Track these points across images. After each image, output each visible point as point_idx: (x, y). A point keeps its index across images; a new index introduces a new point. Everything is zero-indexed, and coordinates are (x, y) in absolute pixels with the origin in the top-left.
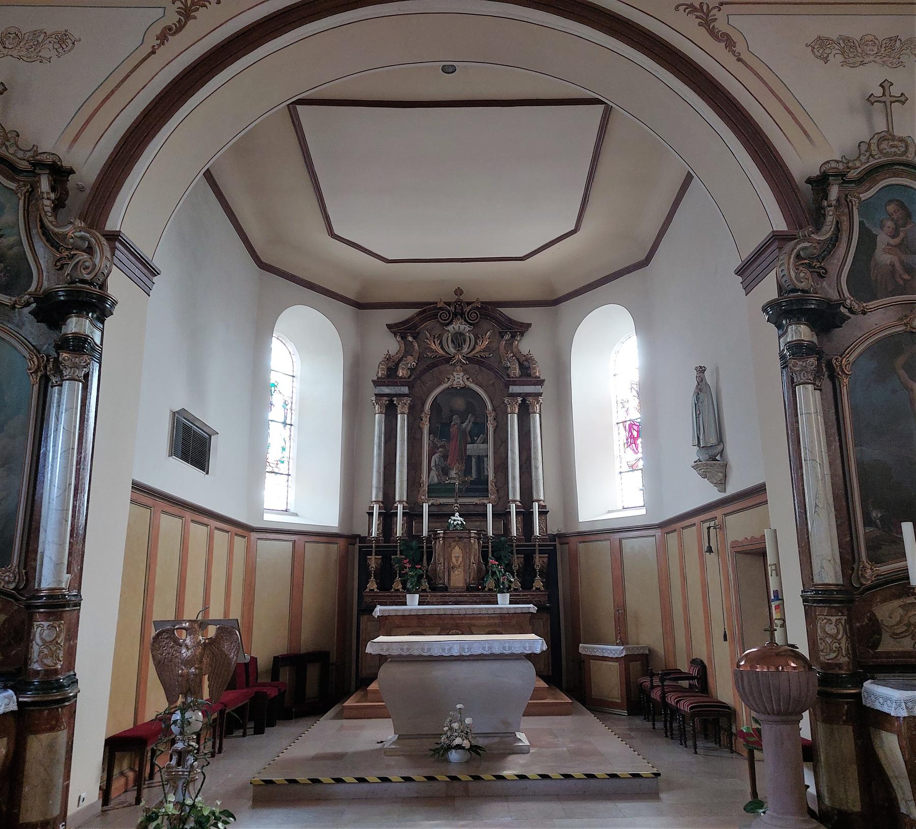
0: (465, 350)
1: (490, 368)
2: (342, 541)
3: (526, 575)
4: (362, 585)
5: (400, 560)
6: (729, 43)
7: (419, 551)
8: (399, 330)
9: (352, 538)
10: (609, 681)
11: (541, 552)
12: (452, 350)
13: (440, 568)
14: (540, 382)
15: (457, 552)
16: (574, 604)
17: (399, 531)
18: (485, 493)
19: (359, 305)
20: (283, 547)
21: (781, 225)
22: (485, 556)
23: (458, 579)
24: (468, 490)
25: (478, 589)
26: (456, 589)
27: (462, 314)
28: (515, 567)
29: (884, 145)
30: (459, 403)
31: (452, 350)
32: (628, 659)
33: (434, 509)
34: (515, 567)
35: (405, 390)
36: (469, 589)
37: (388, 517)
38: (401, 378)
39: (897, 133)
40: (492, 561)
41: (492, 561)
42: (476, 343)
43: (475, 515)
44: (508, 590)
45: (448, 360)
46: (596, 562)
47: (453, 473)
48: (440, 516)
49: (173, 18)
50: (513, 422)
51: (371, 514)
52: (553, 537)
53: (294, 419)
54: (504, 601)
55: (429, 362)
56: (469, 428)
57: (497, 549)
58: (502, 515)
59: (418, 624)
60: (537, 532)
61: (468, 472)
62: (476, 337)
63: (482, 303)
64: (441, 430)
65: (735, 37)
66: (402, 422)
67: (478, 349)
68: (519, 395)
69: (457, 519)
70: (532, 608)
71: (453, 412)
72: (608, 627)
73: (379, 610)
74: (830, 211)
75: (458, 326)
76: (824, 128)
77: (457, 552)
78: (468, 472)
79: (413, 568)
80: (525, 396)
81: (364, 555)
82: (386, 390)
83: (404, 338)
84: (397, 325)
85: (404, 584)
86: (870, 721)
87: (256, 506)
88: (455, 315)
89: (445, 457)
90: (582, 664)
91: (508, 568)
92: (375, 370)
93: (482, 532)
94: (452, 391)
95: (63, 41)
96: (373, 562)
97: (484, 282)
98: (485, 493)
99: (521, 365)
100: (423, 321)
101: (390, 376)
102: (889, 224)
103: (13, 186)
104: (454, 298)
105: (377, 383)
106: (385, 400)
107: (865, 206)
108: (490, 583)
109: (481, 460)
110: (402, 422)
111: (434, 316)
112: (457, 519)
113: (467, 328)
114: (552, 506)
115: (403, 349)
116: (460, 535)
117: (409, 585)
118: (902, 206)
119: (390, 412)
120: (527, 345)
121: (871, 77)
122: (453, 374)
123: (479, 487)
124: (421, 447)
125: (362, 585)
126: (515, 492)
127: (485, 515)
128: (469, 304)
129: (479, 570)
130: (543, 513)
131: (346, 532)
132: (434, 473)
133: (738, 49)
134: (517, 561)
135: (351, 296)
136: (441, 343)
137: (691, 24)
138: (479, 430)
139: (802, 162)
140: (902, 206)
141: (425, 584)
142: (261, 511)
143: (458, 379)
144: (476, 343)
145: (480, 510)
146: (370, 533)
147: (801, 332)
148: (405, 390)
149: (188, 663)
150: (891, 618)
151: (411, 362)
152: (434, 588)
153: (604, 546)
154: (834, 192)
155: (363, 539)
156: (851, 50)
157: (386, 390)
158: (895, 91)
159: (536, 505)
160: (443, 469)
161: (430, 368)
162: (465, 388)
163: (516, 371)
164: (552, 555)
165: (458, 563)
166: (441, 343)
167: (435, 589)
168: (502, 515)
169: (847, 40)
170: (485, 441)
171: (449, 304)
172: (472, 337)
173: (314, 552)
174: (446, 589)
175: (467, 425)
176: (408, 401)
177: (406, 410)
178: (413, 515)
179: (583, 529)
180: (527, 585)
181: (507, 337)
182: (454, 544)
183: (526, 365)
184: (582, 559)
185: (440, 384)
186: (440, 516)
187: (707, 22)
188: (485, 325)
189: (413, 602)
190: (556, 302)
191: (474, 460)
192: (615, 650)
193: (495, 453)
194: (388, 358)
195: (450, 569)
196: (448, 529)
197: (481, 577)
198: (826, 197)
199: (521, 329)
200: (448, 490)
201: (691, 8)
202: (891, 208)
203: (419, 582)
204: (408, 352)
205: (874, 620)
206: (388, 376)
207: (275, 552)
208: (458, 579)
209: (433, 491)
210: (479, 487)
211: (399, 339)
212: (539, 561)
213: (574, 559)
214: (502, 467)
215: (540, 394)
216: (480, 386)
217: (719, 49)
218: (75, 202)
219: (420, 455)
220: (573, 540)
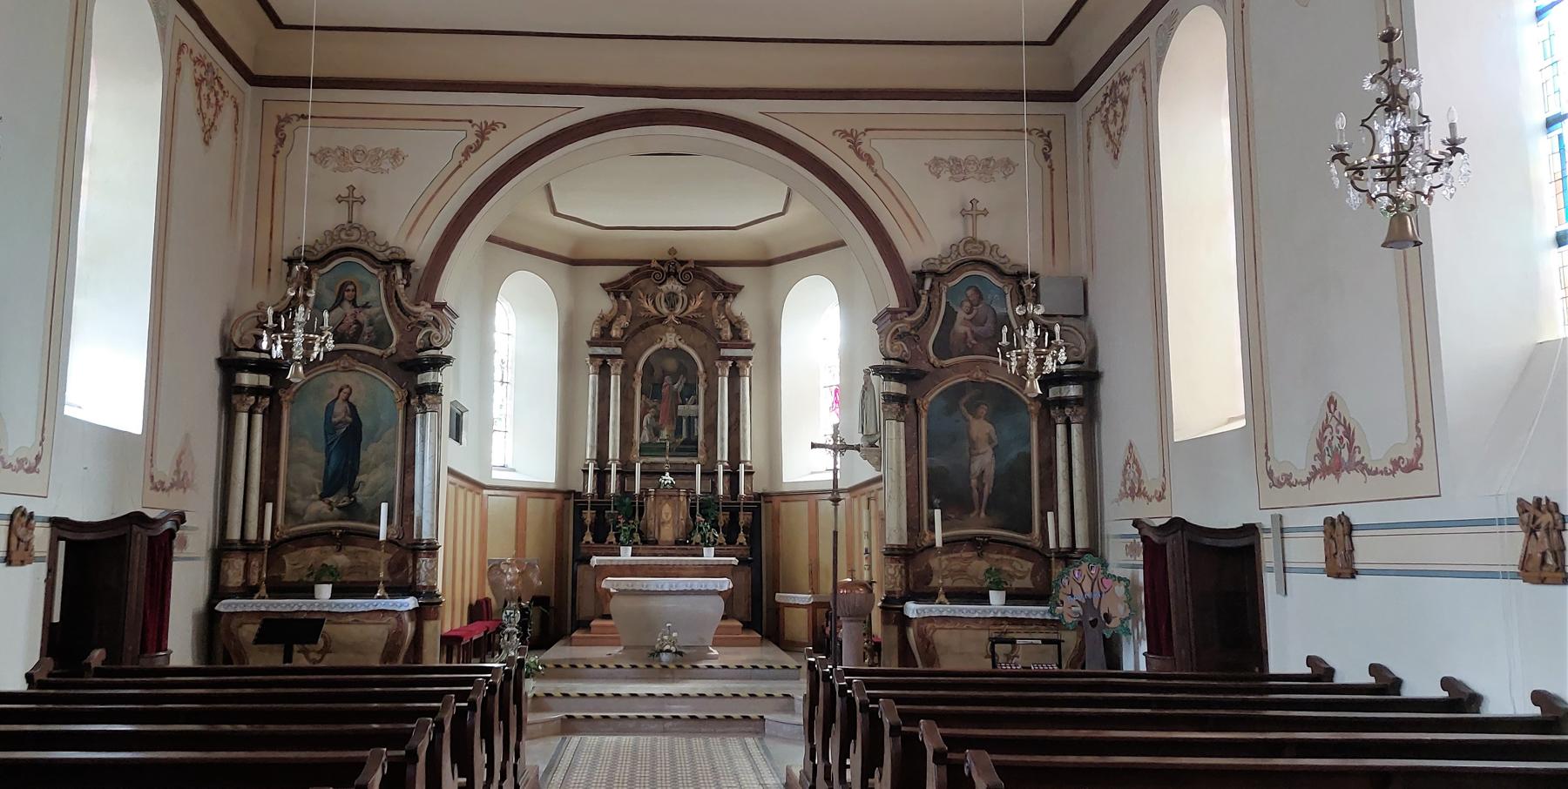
0: (678, 310)
1: (703, 330)
2: (559, 497)
3: (731, 532)
4: (578, 538)
5: (612, 515)
6: (870, 161)
7: (632, 507)
8: (616, 289)
9: (568, 494)
10: (798, 625)
11: (745, 510)
12: (665, 311)
13: (651, 523)
14: (751, 346)
15: (667, 509)
16: (775, 558)
17: (613, 487)
18: (694, 452)
19: (574, 262)
20: (510, 502)
21: (895, 304)
22: (693, 512)
23: (667, 534)
24: (679, 450)
25: (685, 543)
27: (676, 274)
28: (721, 524)
29: (969, 246)
30: (671, 364)
31: (665, 311)
32: (815, 606)
33: (646, 468)
34: (721, 524)
35: (618, 351)
36: (677, 543)
37: (602, 475)
39: (980, 237)
40: (699, 518)
41: (699, 518)
43: (685, 473)
44: (714, 544)
45: (661, 320)
46: (795, 518)
47: (664, 434)
48: (651, 473)
49: (472, 140)
50: (724, 384)
51: (586, 472)
52: (759, 496)
53: (509, 377)
54: (709, 554)
55: (641, 322)
57: (703, 507)
58: (710, 474)
59: (633, 570)
60: (742, 492)
61: (678, 432)
64: (653, 391)
65: (874, 156)
66: (615, 382)
68: (730, 358)
70: (734, 561)
72: (805, 581)
73: (595, 560)
74: (924, 298)
75: (672, 285)
76: (929, 236)
77: (667, 509)
78: (678, 432)
79: (627, 523)
80: (735, 360)
81: (579, 509)
82: (600, 351)
83: (617, 296)
84: (610, 284)
85: (617, 536)
86: (905, 621)
87: (486, 464)
88: (669, 274)
89: (656, 417)
90: (777, 610)
91: (715, 525)
92: (590, 330)
93: (690, 491)
94: (664, 351)
95: (396, 156)
96: (589, 516)
97: (695, 247)
98: (694, 452)
99: (732, 326)
100: (635, 281)
101: (603, 337)
102: (967, 304)
103: (375, 271)
104: (667, 257)
105: (591, 344)
106: (599, 361)
107: (950, 291)
108: (697, 538)
109: (691, 421)
110: (615, 382)
111: (648, 275)
113: (681, 288)
114: (759, 465)
116: (671, 494)
118: (977, 291)
119: (604, 371)
120: (740, 307)
121: (973, 188)
122: (666, 336)
123: (690, 447)
124: (633, 407)
125: (578, 538)
126: (723, 454)
127: (694, 474)
128: (683, 263)
129: (687, 526)
130: (749, 474)
131: (562, 488)
132: (645, 432)
133: (876, 166)
134: (723, 518)
135: (564, 254)
137: (843, 146)
138: (690, 392)
139: (913, 255)
140: (977, 291)
141: (637, 538)
142: (490, 468)
143: (671, 340)
145: (689, 468)
146: (585, 489)
147: (896, 387)
148: (618, 351)
149: (511, 583)
151: (624, 321)
152: (645, 542)
153: (802, 506)
154: (928, 283)
155: (577, 495)
156: (958, 168)
157: (600, 351)
158: (980, 207)
159: (742, 466)
161: (643, 327)
162: (677, 349)
163: (727, 333)
164: (756, 512)
165: (667, 519)
167: (646, 541)
168: (710, 474)
169: (955, 159)
170: (696, 403)
171: (661, 262)
173: (534, 506)
174: (656, 543)
175: (678, 386)
176: (621, 362)
178: (626, 473)
179: (786, 489)
180: (731, 540)
181: (720, 298)
183: (737, 327)
184: (783, 518)
186: (651, 473)
187: (855, 145)
188: (699, 284)
189: (626, 554)
190: (769, 263)
192: (805, 598)
193: (705, 414)
194: (602, 318)
195: (661, 524)
197: (689, 532)
198: (922, 287)
199: (731, 291)
200: (659, 449)
201: (844, 134)
202: (969, 292)
203: (631, 536)
204: (621, 310)
205: (929, 567)
206: (602, 336)
207: (500, 506)
208: (667, 534)
209: (644, 450)
210: (690, 447)
212: (744, 518)
213: (776, 519)
214: (711, 429)
215: (750, 358)
216: (693, 347)
217: (862, 166)
218: (416, 278)
219: (633, 415)
220: (776, 500)
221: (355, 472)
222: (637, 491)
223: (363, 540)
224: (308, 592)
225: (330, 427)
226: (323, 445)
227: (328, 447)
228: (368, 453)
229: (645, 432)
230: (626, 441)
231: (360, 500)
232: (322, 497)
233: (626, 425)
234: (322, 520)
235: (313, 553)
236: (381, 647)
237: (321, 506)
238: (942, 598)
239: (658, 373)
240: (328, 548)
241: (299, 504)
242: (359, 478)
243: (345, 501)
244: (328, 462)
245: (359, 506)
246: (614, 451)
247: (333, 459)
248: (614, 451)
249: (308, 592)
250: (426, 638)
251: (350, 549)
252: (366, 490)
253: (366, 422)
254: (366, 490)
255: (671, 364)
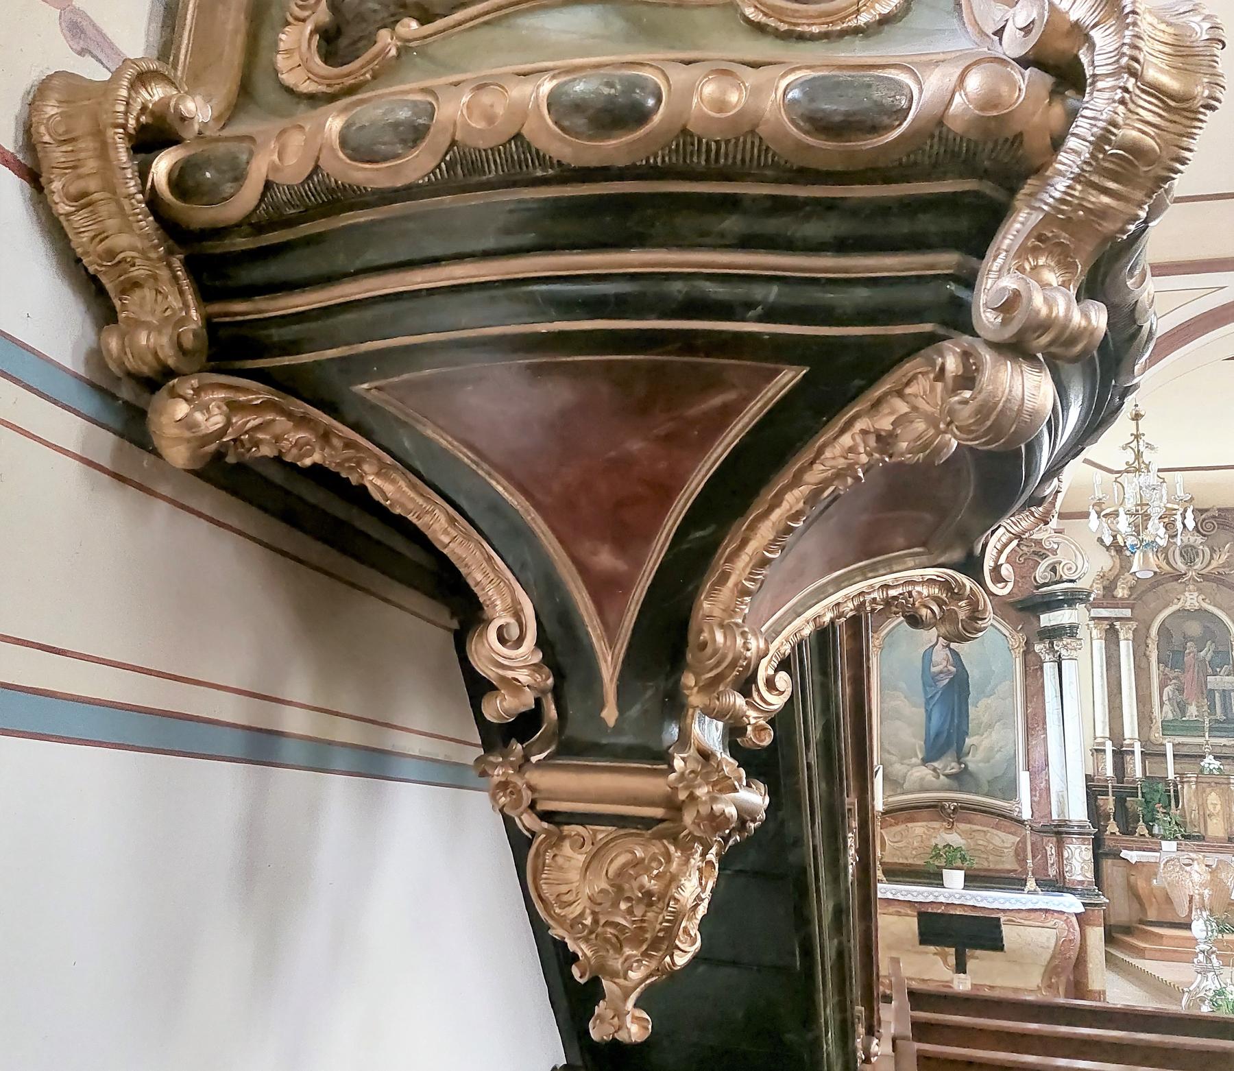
12: (1181, 566)
26: (1216, 839)
31: (1181, 566)
35: (1127, 613)
37: (1120, 755)
38: (1121, 599)
42: (1212, 558)
47: (1192, 710)
56: (1208, 658)
62: (1213, 551)
63: (1219, 510)
64: (1173, 658)
67: (1214, 564)
69: (1210, 762)
71: (1187, 638)
78: (1212, 707)
82: (1104, 613)
89: (1180, 690)
94: (1184, 613)
112: (1210, 762)
115: (1118, 566)
117: (1156, 830)
127: (1165, 755)
132: (1167, 708)
136: (1166, 558)
143: (1191, 600)
144: (1212, 558)
148: (1127, 613)
150: (748, 650)
157: (1104, 613)
160: (1178, 704)
162: (1200, 610)
166: (1166, 558)
172: (1207, 550)
175: (1207, 653)
176: (1134, 625)
177: (1130, 636)
182: (1208, 790)
185: (1165, 607)
191: (1217, 695)
195: (1205, 817)
196: (1201, 772)
200: (1193, 728)
209: (1167, 728)
211: (1113, 553)
221: (963, 733)
222: (1171, 776)
223: (979, 816)
224: (934, 878)
225: (929, 679)
226: (922, 700)
227: (927, 702)
228: (978, 711)
229: (1167, 708)
230: (1145, 718)
231: (971, 767)
232: (925, 761)
233: (1143, 700)
234: (927, 790)
235: (918, 828)
236: (1047, 956)
237: (925, 772)
238: (1031, 884)
239: (1177, 639)
240: (936, 825)
241: (898, 769)
242: (968, 741)
243: (953, 768)
244: (929, 718)
245: (971, 774)
246: (1130, 729)
247: (935, 717)
248: (1130, 729)
249: (934, 878)
250: (1089, 949)
251: (963, 826)
252: (980, 755)
253: (974, 674)
254: (980, 755)
255: (1194, 628)
